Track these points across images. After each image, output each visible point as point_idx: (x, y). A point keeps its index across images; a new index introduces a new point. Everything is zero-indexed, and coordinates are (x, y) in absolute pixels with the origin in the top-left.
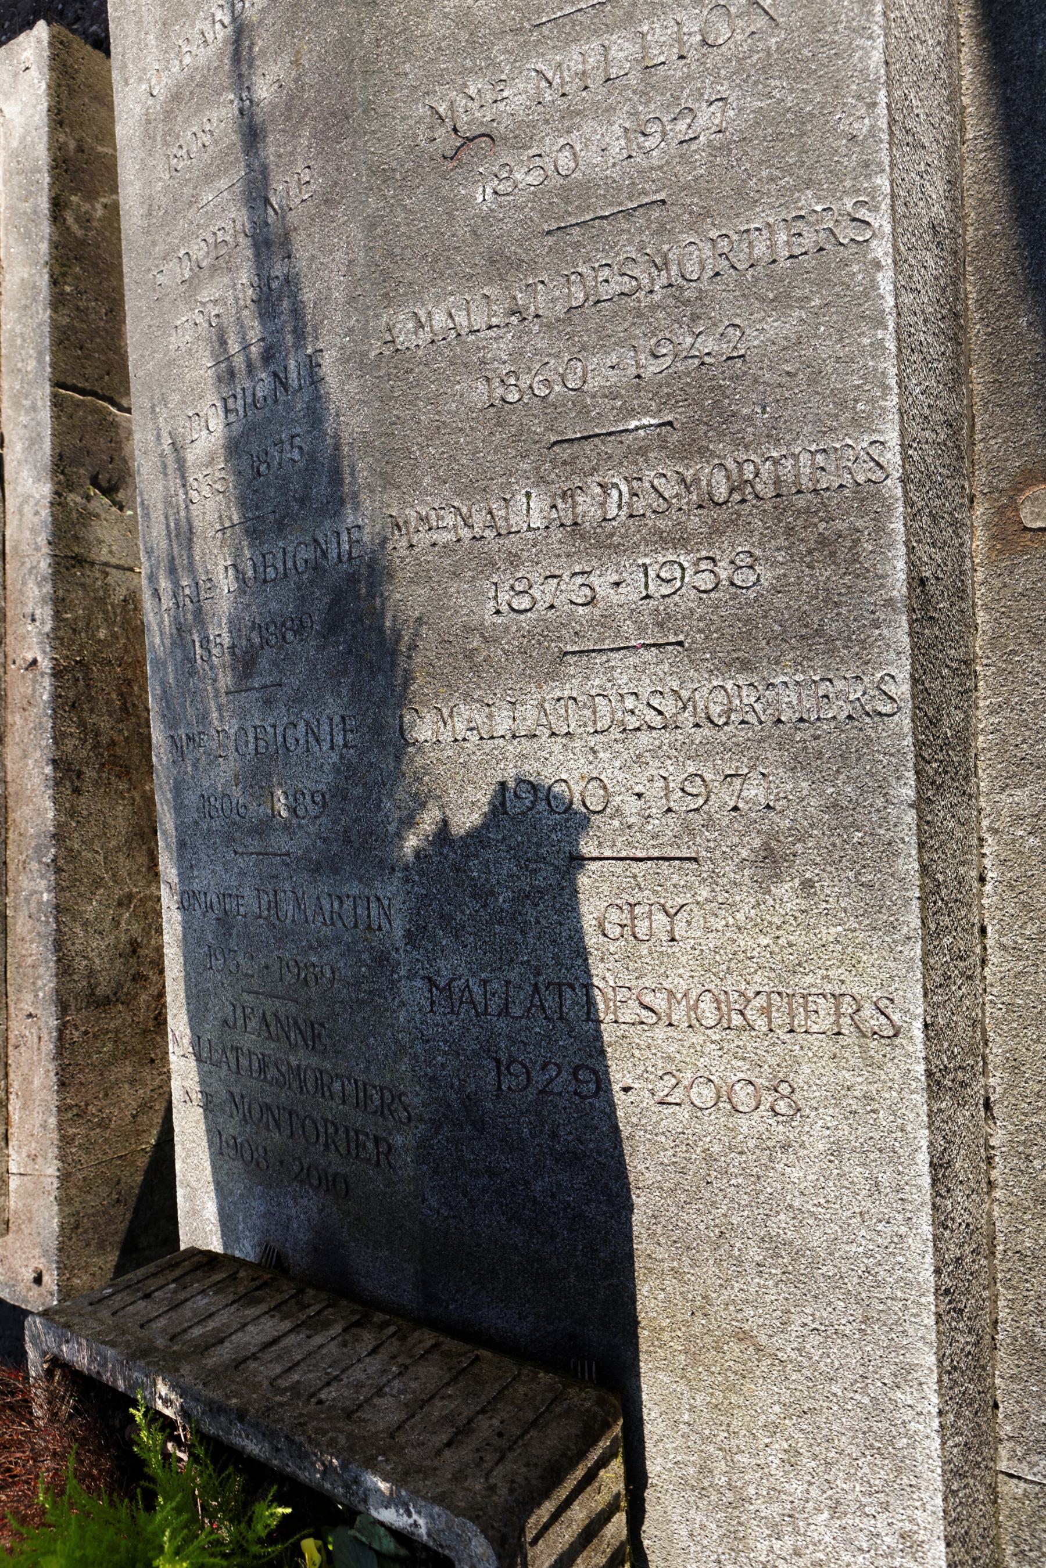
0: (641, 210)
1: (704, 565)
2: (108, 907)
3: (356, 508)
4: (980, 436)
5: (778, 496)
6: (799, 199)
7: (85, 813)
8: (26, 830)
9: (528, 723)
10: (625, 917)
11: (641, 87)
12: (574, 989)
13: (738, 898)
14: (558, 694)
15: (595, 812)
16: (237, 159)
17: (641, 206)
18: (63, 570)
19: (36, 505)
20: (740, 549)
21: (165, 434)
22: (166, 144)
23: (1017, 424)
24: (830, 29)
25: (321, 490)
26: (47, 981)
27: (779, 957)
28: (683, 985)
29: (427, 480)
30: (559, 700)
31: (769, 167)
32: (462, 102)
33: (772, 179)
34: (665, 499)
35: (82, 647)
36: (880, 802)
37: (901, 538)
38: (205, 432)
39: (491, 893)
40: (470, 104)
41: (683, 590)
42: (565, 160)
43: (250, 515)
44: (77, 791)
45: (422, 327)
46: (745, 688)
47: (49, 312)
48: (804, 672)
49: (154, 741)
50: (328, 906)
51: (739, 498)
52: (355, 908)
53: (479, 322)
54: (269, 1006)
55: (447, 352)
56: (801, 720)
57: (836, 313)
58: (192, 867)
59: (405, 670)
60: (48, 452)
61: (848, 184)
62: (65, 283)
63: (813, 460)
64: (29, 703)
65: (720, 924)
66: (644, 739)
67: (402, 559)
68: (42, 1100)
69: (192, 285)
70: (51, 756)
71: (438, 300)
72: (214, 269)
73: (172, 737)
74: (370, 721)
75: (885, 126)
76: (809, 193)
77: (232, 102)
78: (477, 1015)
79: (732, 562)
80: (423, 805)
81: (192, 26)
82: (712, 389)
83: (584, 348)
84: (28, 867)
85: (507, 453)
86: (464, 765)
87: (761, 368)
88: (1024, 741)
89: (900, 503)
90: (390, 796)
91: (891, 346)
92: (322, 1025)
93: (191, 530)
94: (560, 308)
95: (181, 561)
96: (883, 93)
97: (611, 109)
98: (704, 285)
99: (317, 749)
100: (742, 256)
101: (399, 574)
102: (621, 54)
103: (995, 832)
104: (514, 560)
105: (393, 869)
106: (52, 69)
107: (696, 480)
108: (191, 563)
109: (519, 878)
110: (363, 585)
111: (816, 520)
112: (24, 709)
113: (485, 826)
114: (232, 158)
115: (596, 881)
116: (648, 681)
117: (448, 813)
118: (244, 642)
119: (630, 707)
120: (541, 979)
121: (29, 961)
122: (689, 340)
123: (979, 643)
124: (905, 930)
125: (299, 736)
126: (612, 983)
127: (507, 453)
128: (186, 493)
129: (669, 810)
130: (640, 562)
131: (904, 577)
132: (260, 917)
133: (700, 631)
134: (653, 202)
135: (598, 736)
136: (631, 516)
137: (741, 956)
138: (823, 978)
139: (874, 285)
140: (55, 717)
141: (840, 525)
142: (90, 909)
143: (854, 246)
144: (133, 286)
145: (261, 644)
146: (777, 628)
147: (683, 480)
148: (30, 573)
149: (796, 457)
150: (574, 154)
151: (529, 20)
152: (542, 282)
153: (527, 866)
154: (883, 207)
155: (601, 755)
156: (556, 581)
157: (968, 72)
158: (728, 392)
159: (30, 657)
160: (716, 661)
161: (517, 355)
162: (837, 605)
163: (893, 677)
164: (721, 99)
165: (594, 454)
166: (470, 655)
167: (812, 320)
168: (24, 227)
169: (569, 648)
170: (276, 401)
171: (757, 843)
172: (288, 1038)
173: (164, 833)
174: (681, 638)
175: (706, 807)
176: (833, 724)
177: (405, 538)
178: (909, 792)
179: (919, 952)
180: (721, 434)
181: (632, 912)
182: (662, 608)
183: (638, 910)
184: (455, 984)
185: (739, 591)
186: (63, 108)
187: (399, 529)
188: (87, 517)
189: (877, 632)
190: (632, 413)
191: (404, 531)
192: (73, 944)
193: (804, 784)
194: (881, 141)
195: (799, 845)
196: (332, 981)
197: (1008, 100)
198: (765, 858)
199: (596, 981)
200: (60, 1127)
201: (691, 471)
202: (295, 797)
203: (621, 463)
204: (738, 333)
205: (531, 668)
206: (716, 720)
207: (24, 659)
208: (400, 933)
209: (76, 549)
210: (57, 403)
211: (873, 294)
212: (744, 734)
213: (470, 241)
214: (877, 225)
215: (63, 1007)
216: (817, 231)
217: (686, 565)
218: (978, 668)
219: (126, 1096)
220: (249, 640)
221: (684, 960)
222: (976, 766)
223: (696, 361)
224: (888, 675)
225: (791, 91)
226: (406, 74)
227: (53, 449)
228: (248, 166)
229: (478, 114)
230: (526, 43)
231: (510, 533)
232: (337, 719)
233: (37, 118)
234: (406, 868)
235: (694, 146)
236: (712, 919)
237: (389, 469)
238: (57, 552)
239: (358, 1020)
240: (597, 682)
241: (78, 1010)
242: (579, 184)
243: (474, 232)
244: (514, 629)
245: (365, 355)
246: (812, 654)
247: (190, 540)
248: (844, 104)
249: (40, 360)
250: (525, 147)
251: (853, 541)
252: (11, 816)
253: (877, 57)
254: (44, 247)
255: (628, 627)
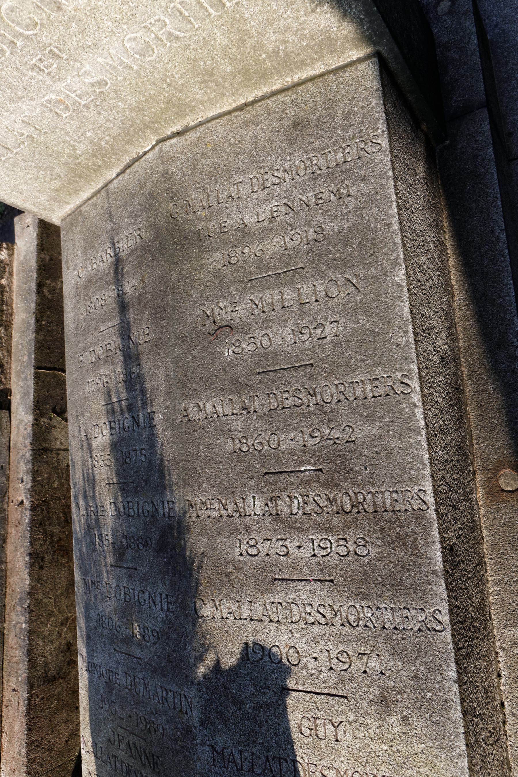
0: (302, 368)
1: (341, 542)
2: (56, 627)
3: (172, 493)
4: (476, 441)
5: (376, 511)
6: (375, 371)
7: (45, 578)
8: (15, 589)
9: (259, 613)
10: (312, 725)
11: (299, 312)
12: (287, 762)
13: (369, 722)
14: (272, 600)
15: (293, 665)
16: (116, 315)
17: (302, 366)
18: (37, 456)
19: (26, 425)
20: (358, 536)
21: (83, 431)
22: (85, 299)
23: (493, 438)
24: (384, 296)
25: (155, 478)
26: (23, 672)
27: (393, 758)
28: (344, 767)
29: (205, 485)
30: (273, 603)
31: (361, 354)
32: (217, 310)
33: (362, 360)
34: (320, 507)
35: (46, 493)
36: (439, 678)
37: (438, 539)
38: (101, 435)
39: (242, 702)
40: (221, 311)
41: (332, 554)
42: (265, 340)
43: (121, 481)
44: (41, 568)
45: (201, 410)
46: (366, 608)
47: (34, 335)
48: (395, 603)
49: (76, 579)
50: (160, 693)
51: (357, 511)
52: (174, 698)
53: (228, 411)
54: (132, 738)
55: (213, 424)
56: (395, 628)
57: (397, 426)
58: (93, 650)
59: (196, 579)
60: (32, 400)
61: (398, 366)
62: (43, 320)
63: (391, 496)
64: (19, 523)
65: (361, 736)
66: (316, 629)
67: (194, 522)
68: (19, 738)
69: (96, 365)
70: (29, 551)
71: (208, 399)
72: (106, 361)
73: (84, 579)
74: (180, 601)
75: (413, 342)
76: (380, 368)
77: (114, 290)
78: (237, 770)
79: (355, 542)
80: (207, 650)
81: (97, 253)
82: (340, 456)
83: (278, 429)
84: (16, 609)
85: (243, 476)
86: (227, 632)
87: (363, 448)
88: (513, 602)
89: (436, 522)
90: (191, 644)
91: (425, 444)
92: (158, 757)
93: (94, 479)
94: (266, 409)
95: (90, 494)
96: (411, 326)
97: (285, 321)
98: (333, 406)
99: (154, 608)
100: (350, 394)
101: (192, 530)
102: (289, 297)
103: (504, 649)
104: (248, 529)
105: (193, 683)
106: (39, 227)
107: (335, 499)
108: (94, 496)
109: (256, 696)
110: (175, 531)
111: (395, 526)
112: (17, 526)
113: (238, 665)
114: (114, 314)
115: (296, 703)
116: (317, 599)
117: (220, 656)
118: (119, 543)
119: (309, 611)
120: (270, 754)
121: (15, 659)
122: (328, 431)
123: (485, 547)
124: (458, 751)
125: (145, 598)
126: (306, 761)
127: (243, 476)
128: (92, 461)
129: (331, 669)
130: (310, 537)
131: (441, 560)
132: (127, 688)
133: (342, 576)
134: (307, 365)
135: (293, 625)
136: (304, 514)
137: (373, 755)
138: (417, 772)
139: (414, 415)
140: (31, 531)
141: (406, 530)
142: (46, 630)
143: (403, 396)
144: (69, 358)
145: (127, 546)
146: (379, 579)
147: (329, 499)
148: (22, 458)
149: (383, 493)
150: (270, 339)
151: (246, 277)
152: (257, 396)
153: (260, 690)
154: (415, 378)
155: (295, 635)
156: (269, 542)
157: (453, 270)
158: (348, 458)
159: (20, 499)
160: (350, 592)
161: (246, 429)
162: (409, 570)
163: (440, 611)
164: (336, 321)
165: (285, 481)
166: (228, 575)
167: (386, 428)
168: (25, 295)
169: (277, 577)
170: (134, 430)
171: (377, 692)
172: (141, 759)
173: (80, 628)
174: (332, 578)
175: (350, 670)
176: (411, 633)
177: (195, 512)
178: (453, 674)
179: (466, 764)
180: (346, 478)
181: (315, 722)
182: (322, 562)
183: (318, 721)
184: (225, 751)
185: (359, 558)
186: (44, 243)
187: (192, 507)
188: (50, 428)
189: (430, 587)
190: (302, 463)
191: (194, 509)
192: (37, 650)
193: (399, 663)
194: (412, 348)
195: (399, 697)
196: (163, 735)
197: (473, 284)
198: (382, 701)
199: (298, 759)
200: (28, 754)
201: (332, 495)
202: (144, 629)
203: (298, 487)
204: (351, 430)
205: (259, 585)
206: (352, 623)
207: (17, 500)
208: (197, 719)
209: (44, 445)
210: (37, 376)
211: (414, 419)
212: (367, 633)
213: (223, 373)
214: (413, 387)
215: (31, 685)
216: (385, 386)
217: (332, 541)
218: (486, 560)
219: (63, 731)
220: (121, 542)
221: (343, 752)
222: (490, 612)
223: (332, 442)
224: (437, 610)
225: (368, 321)
226: (191, 295)
227: (34, 399)
228: (121, 320)
229: (224, 316)
230: (245, 287)
231: (246, 515)
232: (164, 596)
233: (32, 248)
234: (199, 684)
235: (325, 341)
236: (357, 732)
237: (187, 477)
238: (35, 448)
239: (176, 761)
240: (291, 596)
241: (39, 686)
242: (272, 353)
243: (224, 369)
244: (249, 564)
245: (174, 420)
246: (398, 594)
247: (94, 484)
248: (393, 330)
249: (29, 357)
250: (247, 333)
251: (414, 539)
252: (9, 580)
253: (406, 310)
254: (33, 305)
255: (306, 570)
